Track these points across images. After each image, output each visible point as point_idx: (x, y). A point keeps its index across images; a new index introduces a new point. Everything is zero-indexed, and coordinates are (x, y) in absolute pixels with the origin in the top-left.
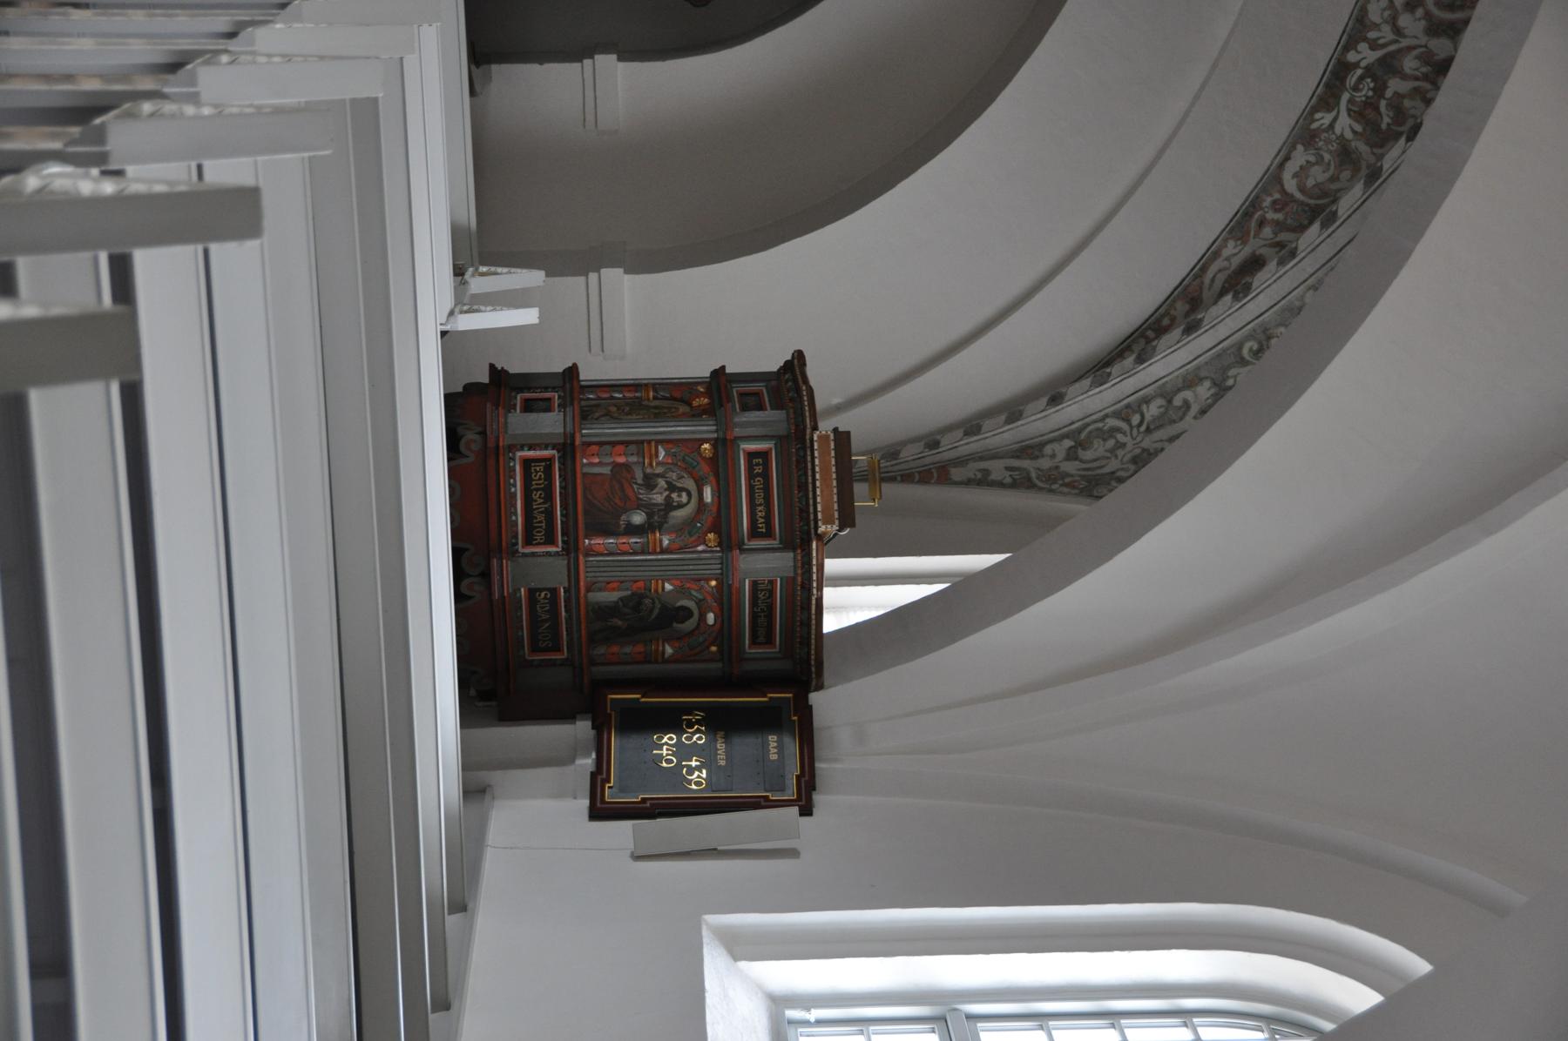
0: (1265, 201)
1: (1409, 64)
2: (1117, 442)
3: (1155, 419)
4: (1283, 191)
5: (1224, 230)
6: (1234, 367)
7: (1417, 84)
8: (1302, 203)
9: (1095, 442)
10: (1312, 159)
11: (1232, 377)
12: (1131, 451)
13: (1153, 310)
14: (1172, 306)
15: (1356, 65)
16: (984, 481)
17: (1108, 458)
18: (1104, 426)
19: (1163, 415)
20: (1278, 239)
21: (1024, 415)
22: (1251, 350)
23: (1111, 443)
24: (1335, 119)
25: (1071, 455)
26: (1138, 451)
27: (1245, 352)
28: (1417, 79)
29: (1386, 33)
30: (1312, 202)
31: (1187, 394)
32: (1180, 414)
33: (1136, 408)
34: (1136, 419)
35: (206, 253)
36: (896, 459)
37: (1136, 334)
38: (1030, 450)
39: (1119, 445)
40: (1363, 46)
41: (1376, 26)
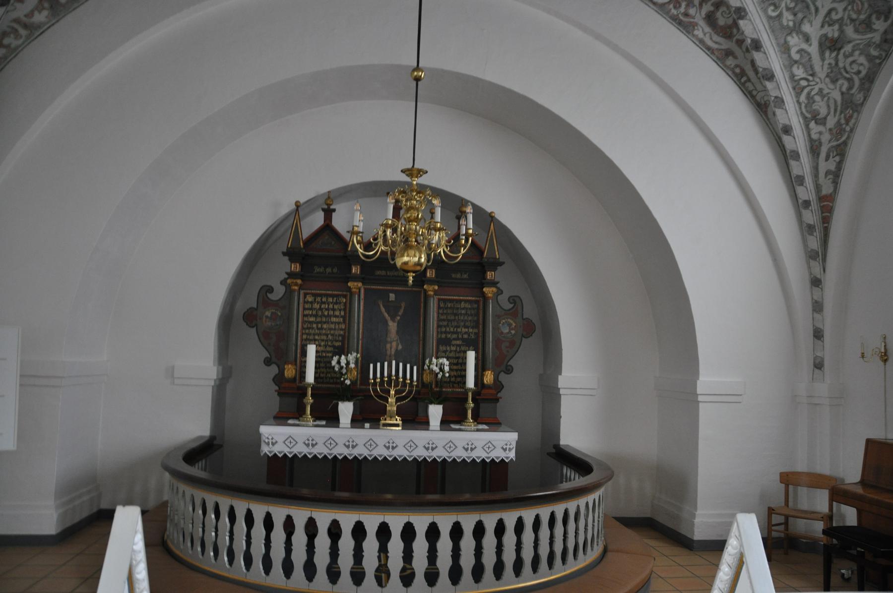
0: (673, 13)
2: (817, 94)
5: (688, 37)
6: (782, 21)
11: (788, 23)
12: (827, 84)
16: (836, 175)
17: (829, 99)
18: (804, 103)
19: (804, 66)
20: (698, 5)
23: (817, 98)
25: (822, 122)
26: (827, 80)
31: (793, 51)
33: (796, 83)
34: (804, 83)
35: (651, 591)
36: (815, 226)
37: (742, 88)
38: (814, 148)
39: (819, 93)
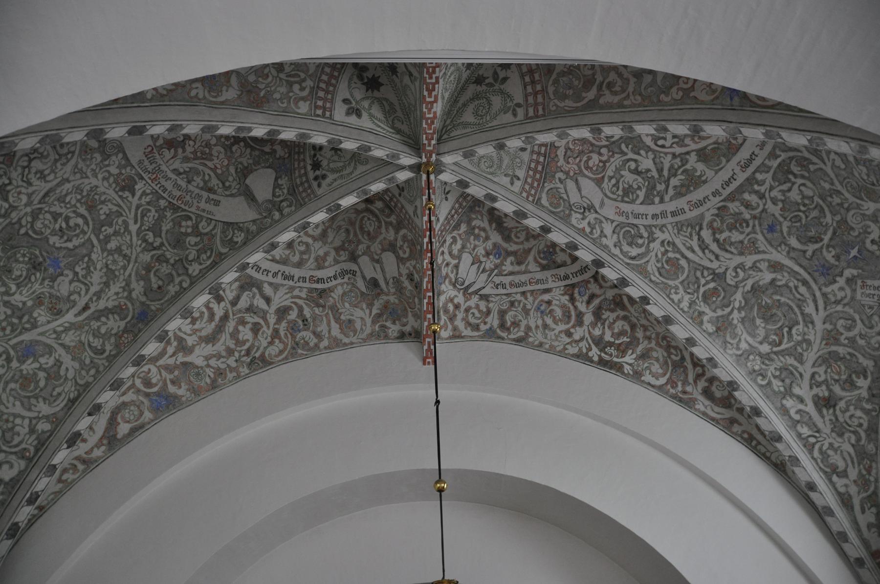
1: (597, 332)
2: (828, 448)
3: (810, 428)
4: (666, 384)
7: (606, 327)
8: (671, 374)
9: (831, 462)
10: (648, 372)
12: (835, 439)
13: (740, 444)
14: (736, 434)
15: (600, 356)
17: (842, 452)
19: (807, 424)
21: (826, 505)
22: (762, 380)
23: (830, 452)
24: (627, 363)
25: (844, 474)
26: (834, 435)
27: (764, 383)
28: (604, 328)
29: (583, 344)
30: (670, 368)
31: (792, 412)
32: (805, 414)
34: (812, 440)
40: (590, 354)
41: (580, 349)
